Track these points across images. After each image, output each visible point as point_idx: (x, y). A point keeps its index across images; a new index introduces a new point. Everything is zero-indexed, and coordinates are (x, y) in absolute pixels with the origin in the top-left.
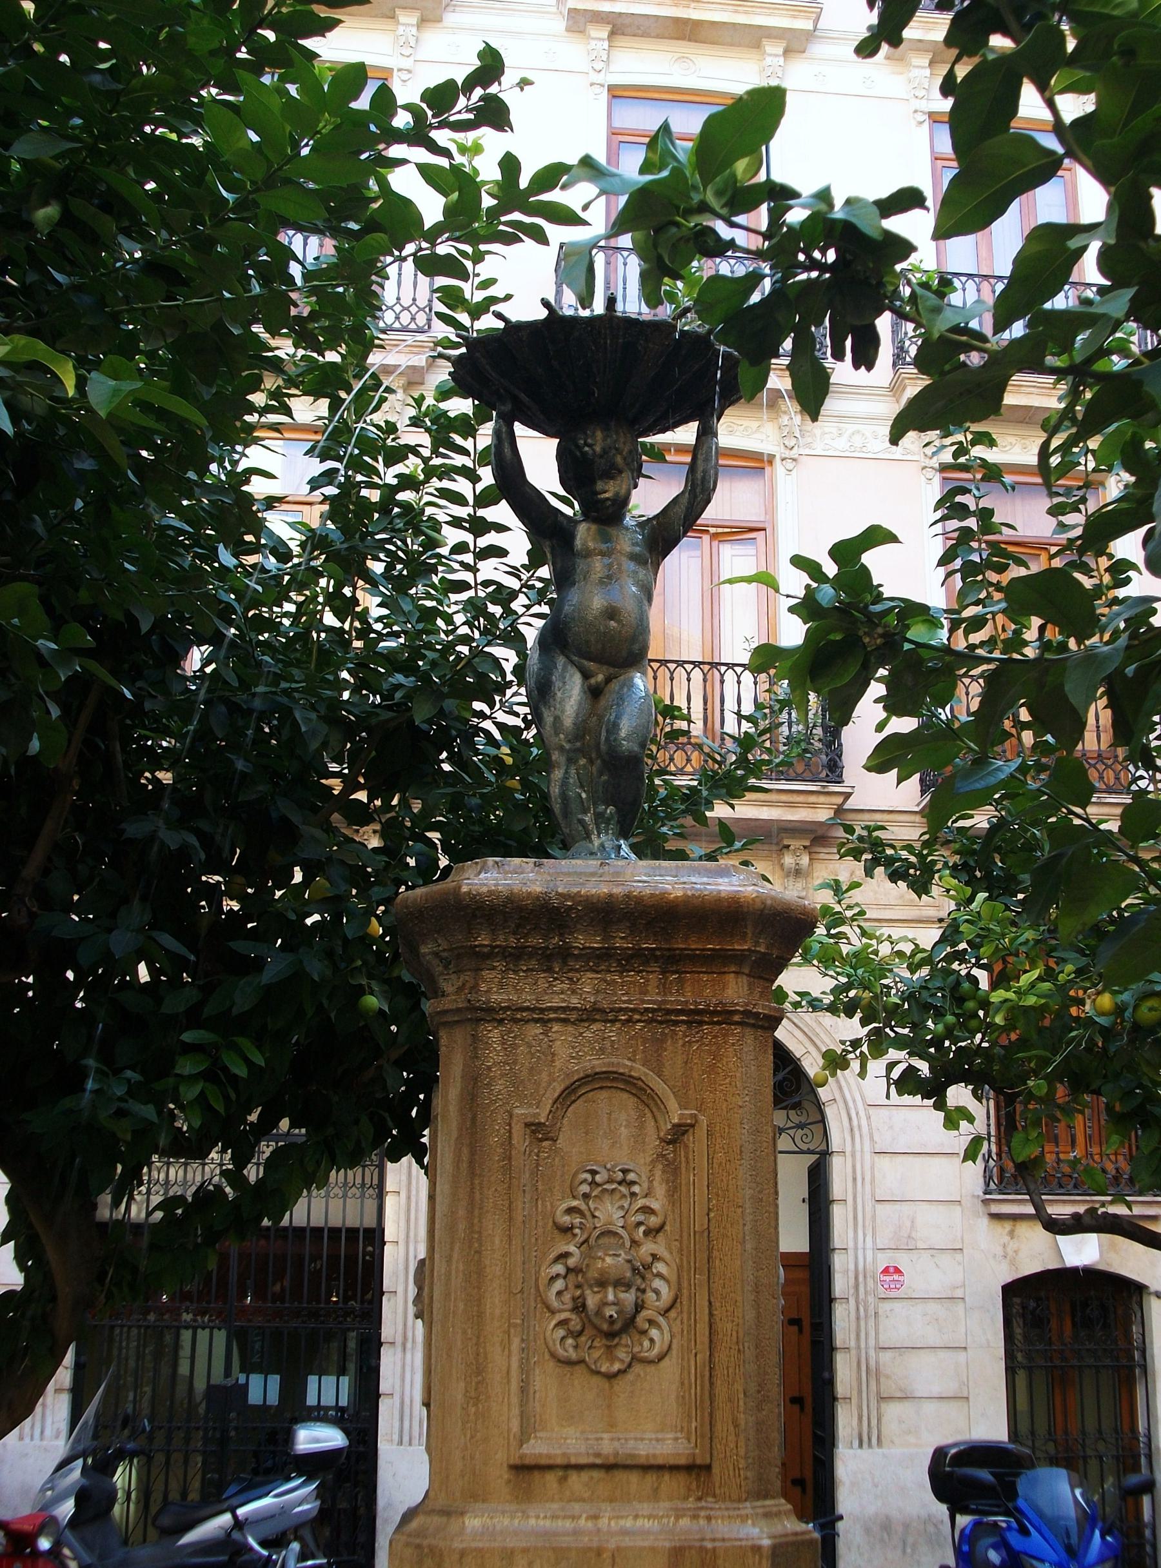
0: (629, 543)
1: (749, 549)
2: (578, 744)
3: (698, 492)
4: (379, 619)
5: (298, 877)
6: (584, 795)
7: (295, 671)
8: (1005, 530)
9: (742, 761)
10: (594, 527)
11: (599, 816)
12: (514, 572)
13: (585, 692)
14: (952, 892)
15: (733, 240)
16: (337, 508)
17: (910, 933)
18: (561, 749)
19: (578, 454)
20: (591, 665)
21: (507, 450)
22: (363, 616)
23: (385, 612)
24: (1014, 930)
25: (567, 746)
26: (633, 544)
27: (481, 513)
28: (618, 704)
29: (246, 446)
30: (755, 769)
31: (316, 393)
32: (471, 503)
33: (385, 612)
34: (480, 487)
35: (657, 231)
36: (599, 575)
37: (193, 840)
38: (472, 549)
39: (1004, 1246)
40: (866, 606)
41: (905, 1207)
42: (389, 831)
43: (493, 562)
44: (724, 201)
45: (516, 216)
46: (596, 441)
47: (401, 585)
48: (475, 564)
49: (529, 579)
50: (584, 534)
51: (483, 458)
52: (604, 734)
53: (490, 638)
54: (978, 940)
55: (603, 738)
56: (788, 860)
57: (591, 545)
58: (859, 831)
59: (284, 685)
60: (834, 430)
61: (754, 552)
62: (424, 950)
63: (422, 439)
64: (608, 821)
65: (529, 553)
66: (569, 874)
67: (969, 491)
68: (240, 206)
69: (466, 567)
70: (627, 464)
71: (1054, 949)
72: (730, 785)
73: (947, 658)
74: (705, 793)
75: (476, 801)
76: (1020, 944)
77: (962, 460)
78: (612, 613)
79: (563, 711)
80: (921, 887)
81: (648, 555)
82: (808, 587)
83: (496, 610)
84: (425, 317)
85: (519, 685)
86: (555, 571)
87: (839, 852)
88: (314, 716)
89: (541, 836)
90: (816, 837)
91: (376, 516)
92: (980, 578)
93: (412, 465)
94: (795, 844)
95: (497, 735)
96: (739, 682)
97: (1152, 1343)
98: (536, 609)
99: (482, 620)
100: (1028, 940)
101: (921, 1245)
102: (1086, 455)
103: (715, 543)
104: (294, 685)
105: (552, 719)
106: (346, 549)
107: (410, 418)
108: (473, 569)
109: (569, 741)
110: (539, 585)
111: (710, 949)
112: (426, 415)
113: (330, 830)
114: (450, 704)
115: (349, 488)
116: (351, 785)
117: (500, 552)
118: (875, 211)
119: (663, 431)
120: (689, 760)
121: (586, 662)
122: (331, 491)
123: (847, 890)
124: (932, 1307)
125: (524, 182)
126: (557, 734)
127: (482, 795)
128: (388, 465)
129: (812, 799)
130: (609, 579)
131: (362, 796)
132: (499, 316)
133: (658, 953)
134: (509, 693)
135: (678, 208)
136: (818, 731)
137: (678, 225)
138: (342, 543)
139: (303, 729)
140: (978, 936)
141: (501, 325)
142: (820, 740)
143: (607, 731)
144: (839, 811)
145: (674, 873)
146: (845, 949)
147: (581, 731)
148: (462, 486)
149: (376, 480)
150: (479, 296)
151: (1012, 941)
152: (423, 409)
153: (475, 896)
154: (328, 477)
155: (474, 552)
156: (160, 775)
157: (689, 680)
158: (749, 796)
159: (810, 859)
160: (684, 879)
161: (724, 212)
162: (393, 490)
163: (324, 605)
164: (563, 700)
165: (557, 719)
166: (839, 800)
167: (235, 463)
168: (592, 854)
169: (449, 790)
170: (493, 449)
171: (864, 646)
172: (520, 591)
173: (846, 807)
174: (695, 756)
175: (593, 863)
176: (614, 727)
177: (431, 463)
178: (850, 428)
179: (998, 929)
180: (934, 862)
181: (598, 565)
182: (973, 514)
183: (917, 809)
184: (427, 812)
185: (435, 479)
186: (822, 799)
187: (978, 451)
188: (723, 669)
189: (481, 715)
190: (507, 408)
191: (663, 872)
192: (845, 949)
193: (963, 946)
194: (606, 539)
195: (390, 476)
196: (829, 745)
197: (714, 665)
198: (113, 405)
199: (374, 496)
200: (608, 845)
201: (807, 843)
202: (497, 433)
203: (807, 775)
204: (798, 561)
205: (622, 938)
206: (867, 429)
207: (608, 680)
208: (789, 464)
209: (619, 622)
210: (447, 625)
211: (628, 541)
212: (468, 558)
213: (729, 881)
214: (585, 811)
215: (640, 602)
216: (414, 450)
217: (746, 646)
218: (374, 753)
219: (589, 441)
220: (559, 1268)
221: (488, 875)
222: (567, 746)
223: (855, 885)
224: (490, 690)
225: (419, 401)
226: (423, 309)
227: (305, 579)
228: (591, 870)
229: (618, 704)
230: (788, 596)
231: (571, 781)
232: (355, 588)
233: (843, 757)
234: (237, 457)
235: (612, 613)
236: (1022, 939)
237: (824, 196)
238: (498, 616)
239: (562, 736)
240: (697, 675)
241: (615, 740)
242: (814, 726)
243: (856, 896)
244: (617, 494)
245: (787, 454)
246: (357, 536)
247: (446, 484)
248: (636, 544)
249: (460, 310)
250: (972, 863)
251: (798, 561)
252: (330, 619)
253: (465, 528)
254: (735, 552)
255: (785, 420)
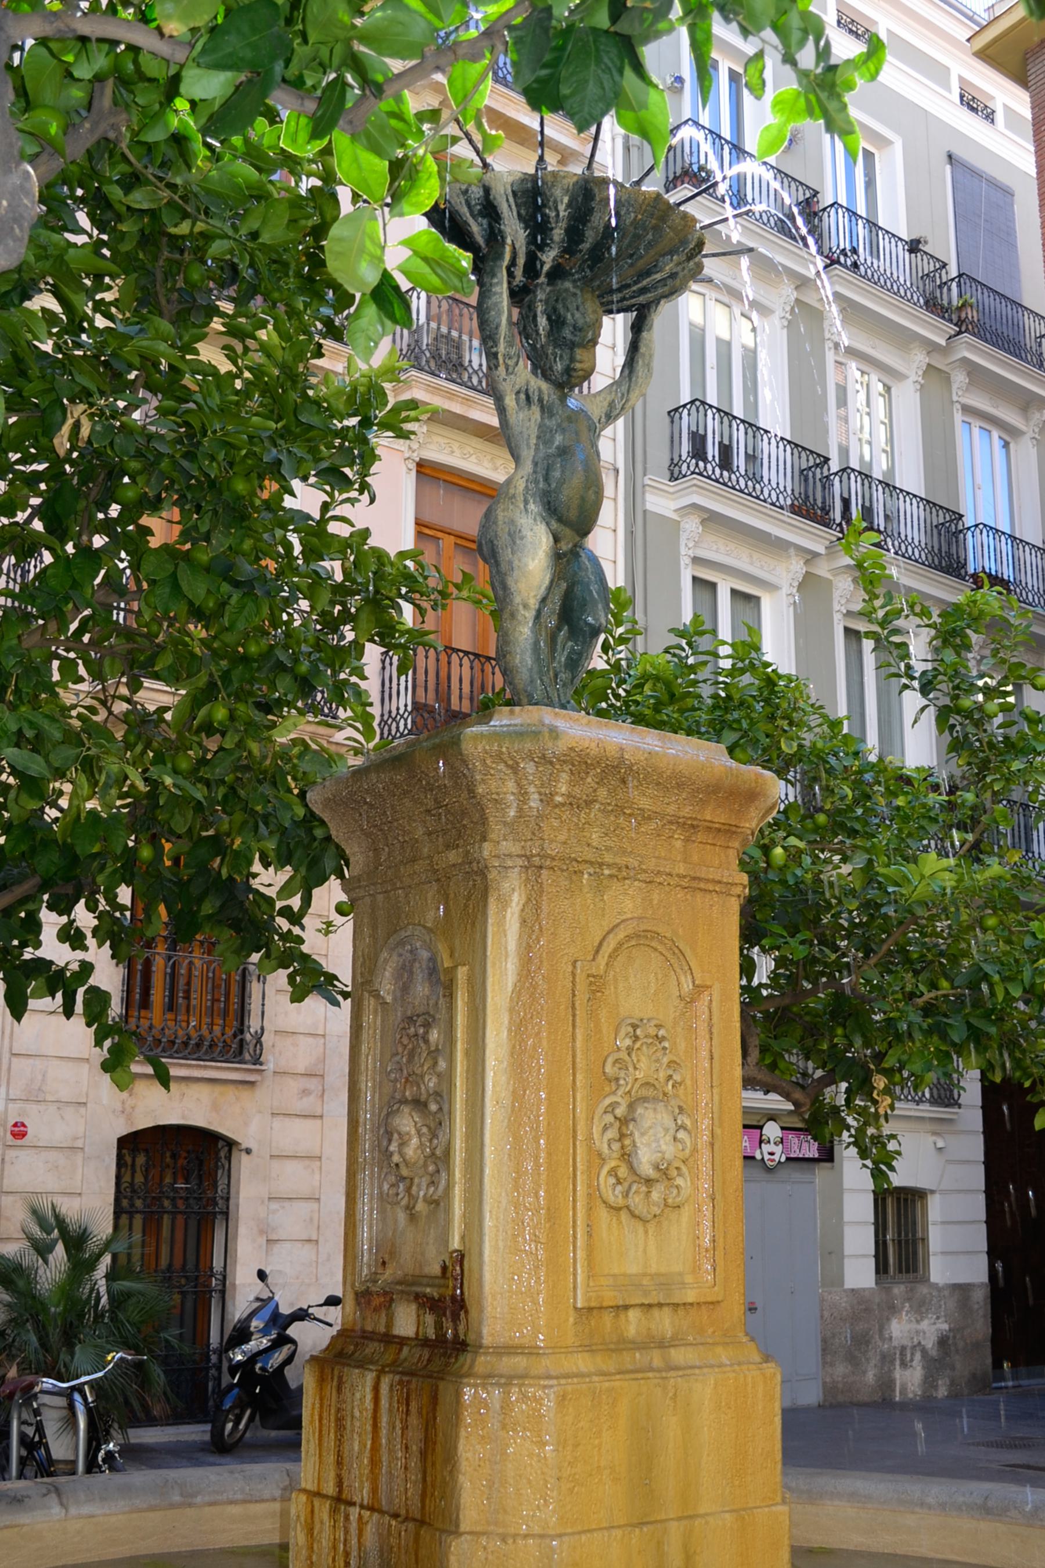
39: (123, 1103)
41: (38, 1062)
97: (238, 1193)
101: (49, 1098)
111: (373, 1097)
124: (52, 1155)
220: (609, 1118)
237: (366, 533)
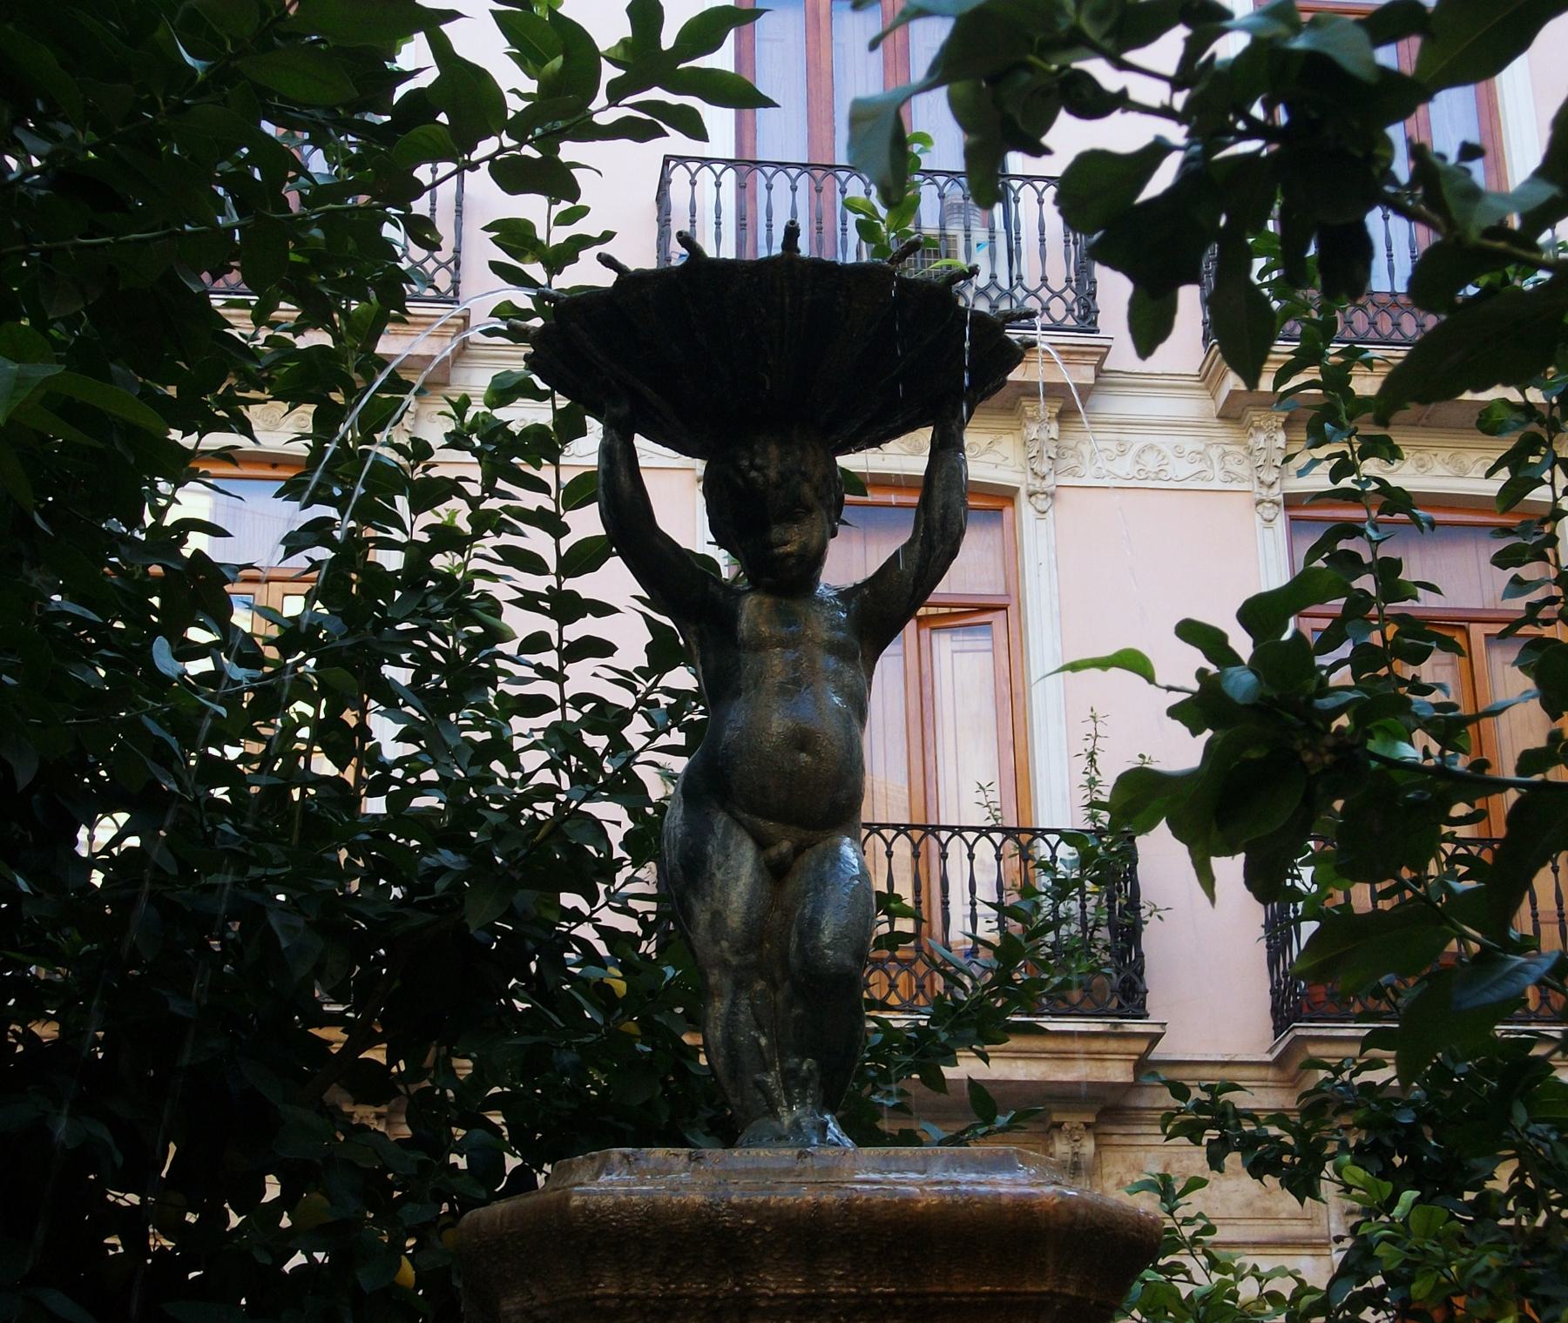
0: (826, 625)
1: (981, 641)
2: (752, 957)
3: (935, 543)
4: (399, 763)
5: (273, 1190)
6: (763, 1041)
7: (272, 848)
8: (1421, 592)
9: (1003, 977)
10: (768, 600)
11: (789, 1076)
12: (625, 680)
13: (761, 871)
14: (1355, 1192)
15: (1124, 93)
16: (329, 587)
17: (1290, 1263)
18: (724, 965)
19: (740, 481)
20: (770, 827)
21: (624, 479)
22: (373, 758)
23: (411, 749)
24: (1466, 1251)
25: (734, 960)
26: (833, 628)
27: (569, 584)
28: (816, 889)
29: (179, 484)
30: (1025, 998)
31: (293, 398)
32: (553, 569)
33: (411, 749)
34: (567, 543)
35: (994, 80)
36: (779, 678)
37: (103, 1133)
38: (556, 644)
40: (1309, 701)
42: (424, 1110)
43: (590, 664)
44: (1106, 26)
45: (656, 94)
46: (769, 462)
47: (438, 705)
48: (562, 668)
49: (649, 691)
50: (752, 612)
51: (576, 494)
52: (794, 939)
53: (590, 788)
54: (1405, 1271)
55: (793, 946)
56: (1061, 1147)
57: (765, 629)
58: (1197, 1094)
59: (255, 872)
60: (1113, 446)
61: (988, 645)
62: (507, 1306)
63: (462, 466)
64: (804, 1084)
65: (649, 649)
66: (747, 1172)
67: (1361, 532)
68: (221, 76)
69: (545, 672)
70: (820, 498)
71: (1535, 1281)
72: (981, 1023)
73: (1441, 785)
74: (943, 1036)
75: (570, 1058)
76: (1477, 1275)
77: (1346, 482)
78: (802, 740)
79: (726, 903)
80: (1303, 1185)
81: (856, 643)
82: (1201, 674)
83: (598, 742)
84: (449, 277)
85: (637, 864)
86: (705, 677)
87: (1164, 1132)
88: (300, 922)
89: (706, 1112)
90: (1108, 1110)
91: (398, 594)
92: (1384, 671)
93: (456, 512)
94: (1072, 1120)
95: (602, 948)
96: (971, 857)
98: (663, 740)
99: (573, 759)
100: (1488, 1270)
102: (1552, 468)
103: (925, 632)
104: (270, 872)
105: (707, 916)
106: (350, 648)
107: (447, 435)
108: (559, 677)
109: (737, 952)
110: (665, 700)
111: (984, 1294)
112: (473, 428)
113: (333, 1114)
114: (525, 898)
115: (351, 552)
116: (361, 1037)
117: (601, 648)
118: (1361, 35)
119: (876, 442)
120: (893, 987)
121: (761, 822)
122: (323, 553)
123: (1183, 1193)
125: (668, 40)
126: (716, 942)
127: (582, 1048)
128: (416, 509)
129: (1097, 1045)
130: (794, 686)
131: (378, 1055)
132: (607, 261)
133: (899, 1302)
134: (620, 877)
135: (1030, 41)
136: (1103, 934)
137: (1029, 67)
138: (342, 638)
139: (284, 944)
140: (1405, 1263)
141: (607, 278)
142: (1106, 948)
143: (800, 933)
144: (1143, 1066)
145: (920, 1166)
146: (1185, 1290)
147: (756, 934)
148: (537, 541)
149: (397, 535)
150: (560, 235)
151: (1463, 1270)
152: (469, 417)
153: (593, 1213)
154: (317, 531)
155: (558, 649)
156: (37, 1029)
157: (889, 855)
158: (1014, 1042)
159: (1097, 1146)
160: (939, 1177)
161: (1108, 44)
162: (428, 551)
163: (310, 742)
164: (725, 884)
165: (717, 916)
166: (1141, 1046)
167: (160, 513)
168: (780, 1138)
169: (528, 1040)
170: (601, 478)
171: (1304, 767)
172: (635, 709)
173: (1153, 1056)
174: (902, 979)
175: (788, 1153)
176: (812, 926)
177: (482, 506)
178: (1137, 441)
179: (1439, 1251)
180: (1322, 1143)
181: (777, 663)
182: (1368, 569)
183: (1269, 1058)
184: (482, 1077)
185: (489, 533)
186: (1113, 1045)
187: (1371, 467)
188: (944, 835)
189: (576, 916)
190: (623, 410)
191: (902, 1165)
192: (1185, 1290)
193: (1378, 1281)
194: (789, 619)
195: (419, 526)
196: (1121, 955)
197: (934, 830)
198: (16, 403)
199: (392, 561)
200: (805, 1122)
201: (1091, 1119)
202: (606, 451)
203: (1087, 1006)
204: (1190, 631)
205: (839, 1278)
206: (1164, 442)
207: (798, 851)
208: (1042, 503)
209: (814, 753)
210: (510, 769)
211: (824, 625)
212: (550, 659)
213: (1010, 1179)
214: (766, 1069)
215: (849, 721)
216: (452, 488)
217: (981, 797)
218: (397, 984)
219: (758, 461)
221: (614, 1177)
222: (734, 960)
223: (1196, 1183)
224: (591, 873)
225: (461, 406)
226: (445, 265)
227: (271, 701)
228: (785, 1165)
229: (816, 889)
230: (1169, 689)
231: (742, 1017)
232: (364, 711)
233: (1146, 976)
234: (163, 502)
235: (802, 740)
236: (1479, 1267)
238: (600, 752)
239: (725, 944)
240: (902, 847)
241: (815, 948)
242: (1097, 926)
243: (1194, 1204)
244: (804, 547)
245: (1038, 485)
246: (369, 626)
247: (506, 539)
248: (838, 627)
249: (529, 257)
250: (1387, 1142)
251: (1190, 631)
252: (323, 766)
253: (542, 611)
254: (957, 646)
255: (1033, 430)
